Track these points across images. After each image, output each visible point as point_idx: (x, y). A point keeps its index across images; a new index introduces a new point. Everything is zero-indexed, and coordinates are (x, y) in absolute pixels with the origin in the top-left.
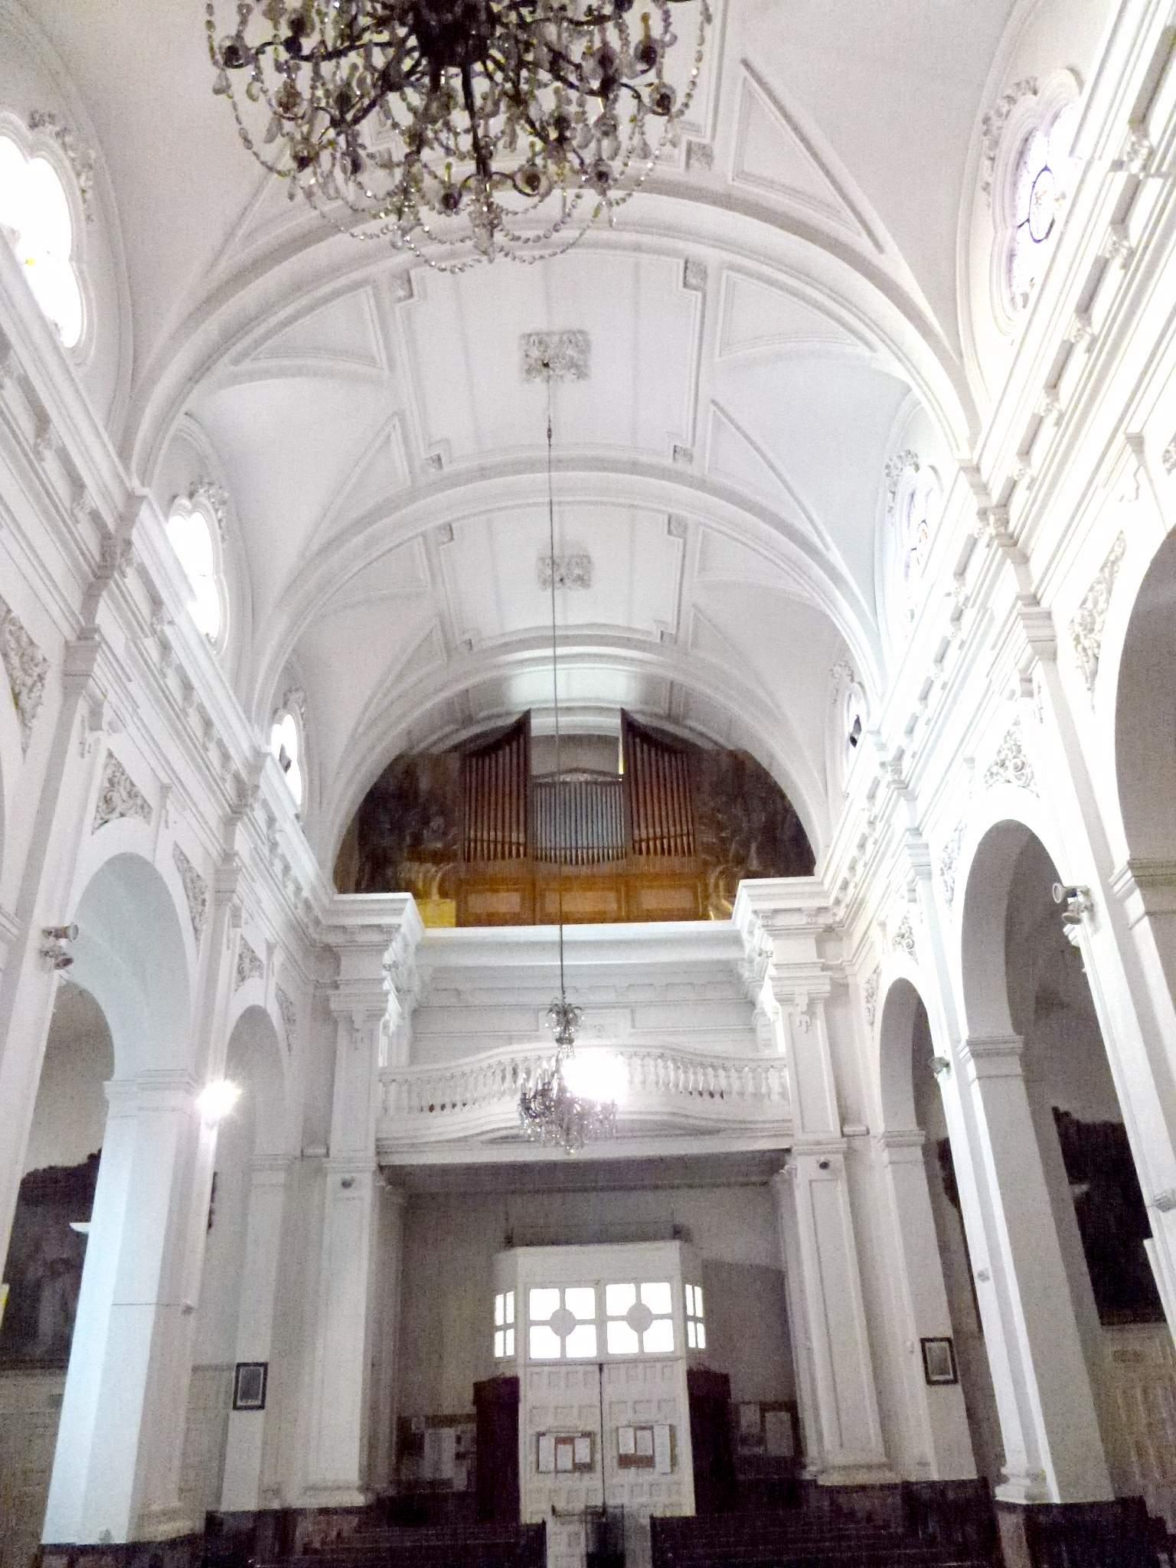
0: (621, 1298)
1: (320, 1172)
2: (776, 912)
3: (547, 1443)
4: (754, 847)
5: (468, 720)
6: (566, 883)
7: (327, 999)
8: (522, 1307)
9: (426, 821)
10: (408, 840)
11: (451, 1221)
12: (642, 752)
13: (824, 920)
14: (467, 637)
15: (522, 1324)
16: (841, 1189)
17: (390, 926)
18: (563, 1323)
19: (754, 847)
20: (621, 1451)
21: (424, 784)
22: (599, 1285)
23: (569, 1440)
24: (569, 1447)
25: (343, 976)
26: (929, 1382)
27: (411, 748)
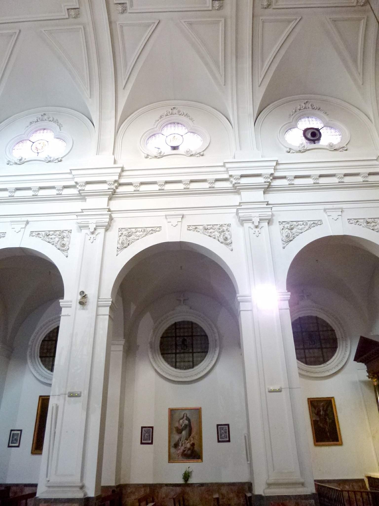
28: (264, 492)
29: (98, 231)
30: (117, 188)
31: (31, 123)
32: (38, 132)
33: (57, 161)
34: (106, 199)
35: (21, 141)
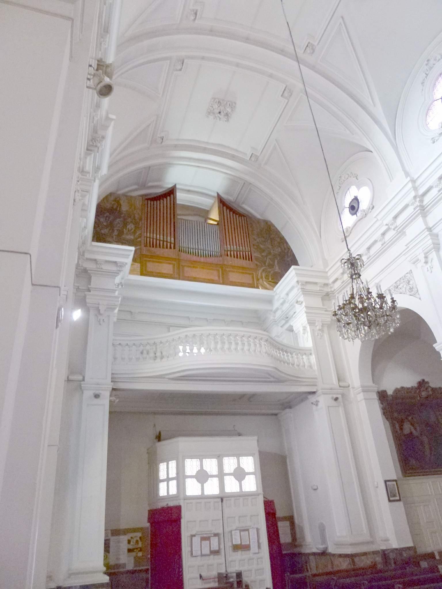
0: (230, 464)
1: (80, 389)
2: (307, 283)
3: (196, 540)
4: (276, 261)
5: (144, 186)
6: (194, 264)
7: (85, 297)
8: (181, 469)
9: (125, 225)
10: (116, 233)
11: (150, 418)
12: (226, 212)
13: (327, 289)
14: (162, 135)
15: (181, 478)
16: (341, 410)
17: (123, 263)
18: (202, 477)
19: (276, 261)
20: (234, 543)
21: (125, 208)
22: (220, 458)
23: (208, 539)
24: (208, 542)
25: (93, 285)
26: (390, 501)
27: (117, 190)
28: (317, 549)
29: (430, 257)
30: (421, 201)
31: (423, 83)
32: (437, 83)
33: (370, 210)
34: (420, 219)
35: (428, 109)
